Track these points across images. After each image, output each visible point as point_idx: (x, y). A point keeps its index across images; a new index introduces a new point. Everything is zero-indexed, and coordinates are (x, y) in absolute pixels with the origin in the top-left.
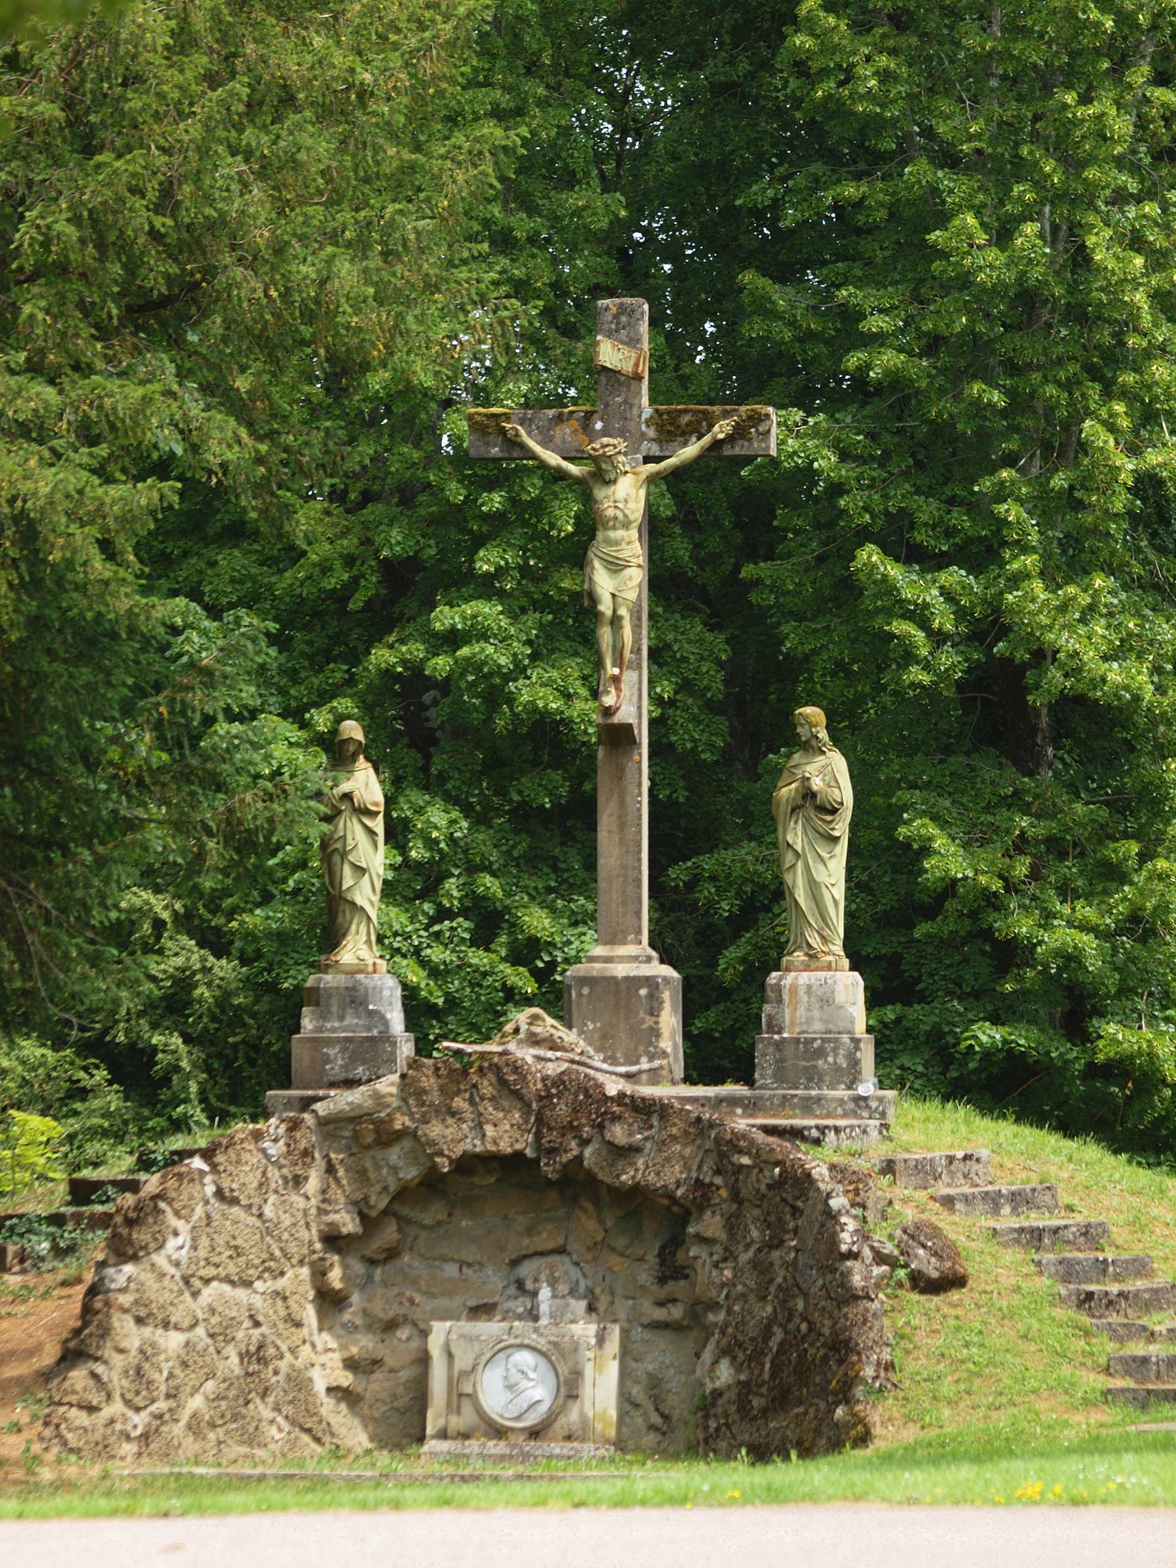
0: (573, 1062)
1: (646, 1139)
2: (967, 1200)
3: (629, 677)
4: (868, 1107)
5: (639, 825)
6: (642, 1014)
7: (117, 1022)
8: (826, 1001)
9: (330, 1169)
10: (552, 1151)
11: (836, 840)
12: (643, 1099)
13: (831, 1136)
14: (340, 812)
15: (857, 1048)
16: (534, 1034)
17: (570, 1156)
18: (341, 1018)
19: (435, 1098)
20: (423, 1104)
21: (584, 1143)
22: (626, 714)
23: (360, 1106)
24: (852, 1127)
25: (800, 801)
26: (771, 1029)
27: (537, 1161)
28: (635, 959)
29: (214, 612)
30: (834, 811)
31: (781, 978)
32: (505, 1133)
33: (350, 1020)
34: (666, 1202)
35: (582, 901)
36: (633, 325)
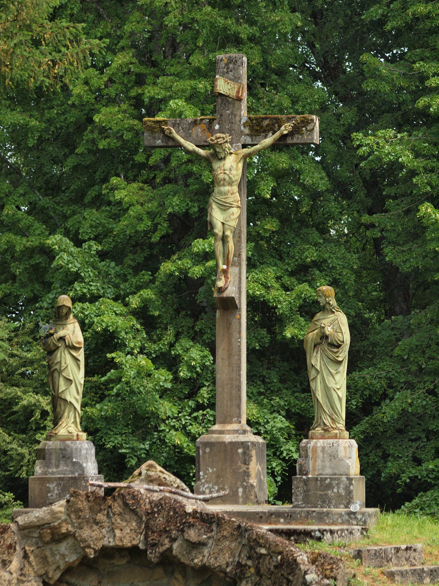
0: (171, 492)
1: (209, 538)
2: (402, 574)
3: (233, 271)
4: (356, 518)
7: (22, 466)
8: (333, 456)
9: (26, 556)
10: (154, 545)
11: (340, 363)
12: (207, 514)
13: (328, 536)
14: (58, 348)
15: (351, 484)
16: (149, 476)
17: (164, 548)
18: (57, 466)
19: (87, 514)
20: (79, 517)
21: (173, 540)
22: (231, 292)
23: (43, 519)
24: (342, 530)
25: (319, 341)
26: (301, 473)
27: (146, 551)
28: (236, 432)
29: (78, 243)
30: (339, 346)
31: (307, 443)
32: (127, 534)
33: (62, 468)
34: (222, 575)
35: (278, 399)
36: (236, 69)
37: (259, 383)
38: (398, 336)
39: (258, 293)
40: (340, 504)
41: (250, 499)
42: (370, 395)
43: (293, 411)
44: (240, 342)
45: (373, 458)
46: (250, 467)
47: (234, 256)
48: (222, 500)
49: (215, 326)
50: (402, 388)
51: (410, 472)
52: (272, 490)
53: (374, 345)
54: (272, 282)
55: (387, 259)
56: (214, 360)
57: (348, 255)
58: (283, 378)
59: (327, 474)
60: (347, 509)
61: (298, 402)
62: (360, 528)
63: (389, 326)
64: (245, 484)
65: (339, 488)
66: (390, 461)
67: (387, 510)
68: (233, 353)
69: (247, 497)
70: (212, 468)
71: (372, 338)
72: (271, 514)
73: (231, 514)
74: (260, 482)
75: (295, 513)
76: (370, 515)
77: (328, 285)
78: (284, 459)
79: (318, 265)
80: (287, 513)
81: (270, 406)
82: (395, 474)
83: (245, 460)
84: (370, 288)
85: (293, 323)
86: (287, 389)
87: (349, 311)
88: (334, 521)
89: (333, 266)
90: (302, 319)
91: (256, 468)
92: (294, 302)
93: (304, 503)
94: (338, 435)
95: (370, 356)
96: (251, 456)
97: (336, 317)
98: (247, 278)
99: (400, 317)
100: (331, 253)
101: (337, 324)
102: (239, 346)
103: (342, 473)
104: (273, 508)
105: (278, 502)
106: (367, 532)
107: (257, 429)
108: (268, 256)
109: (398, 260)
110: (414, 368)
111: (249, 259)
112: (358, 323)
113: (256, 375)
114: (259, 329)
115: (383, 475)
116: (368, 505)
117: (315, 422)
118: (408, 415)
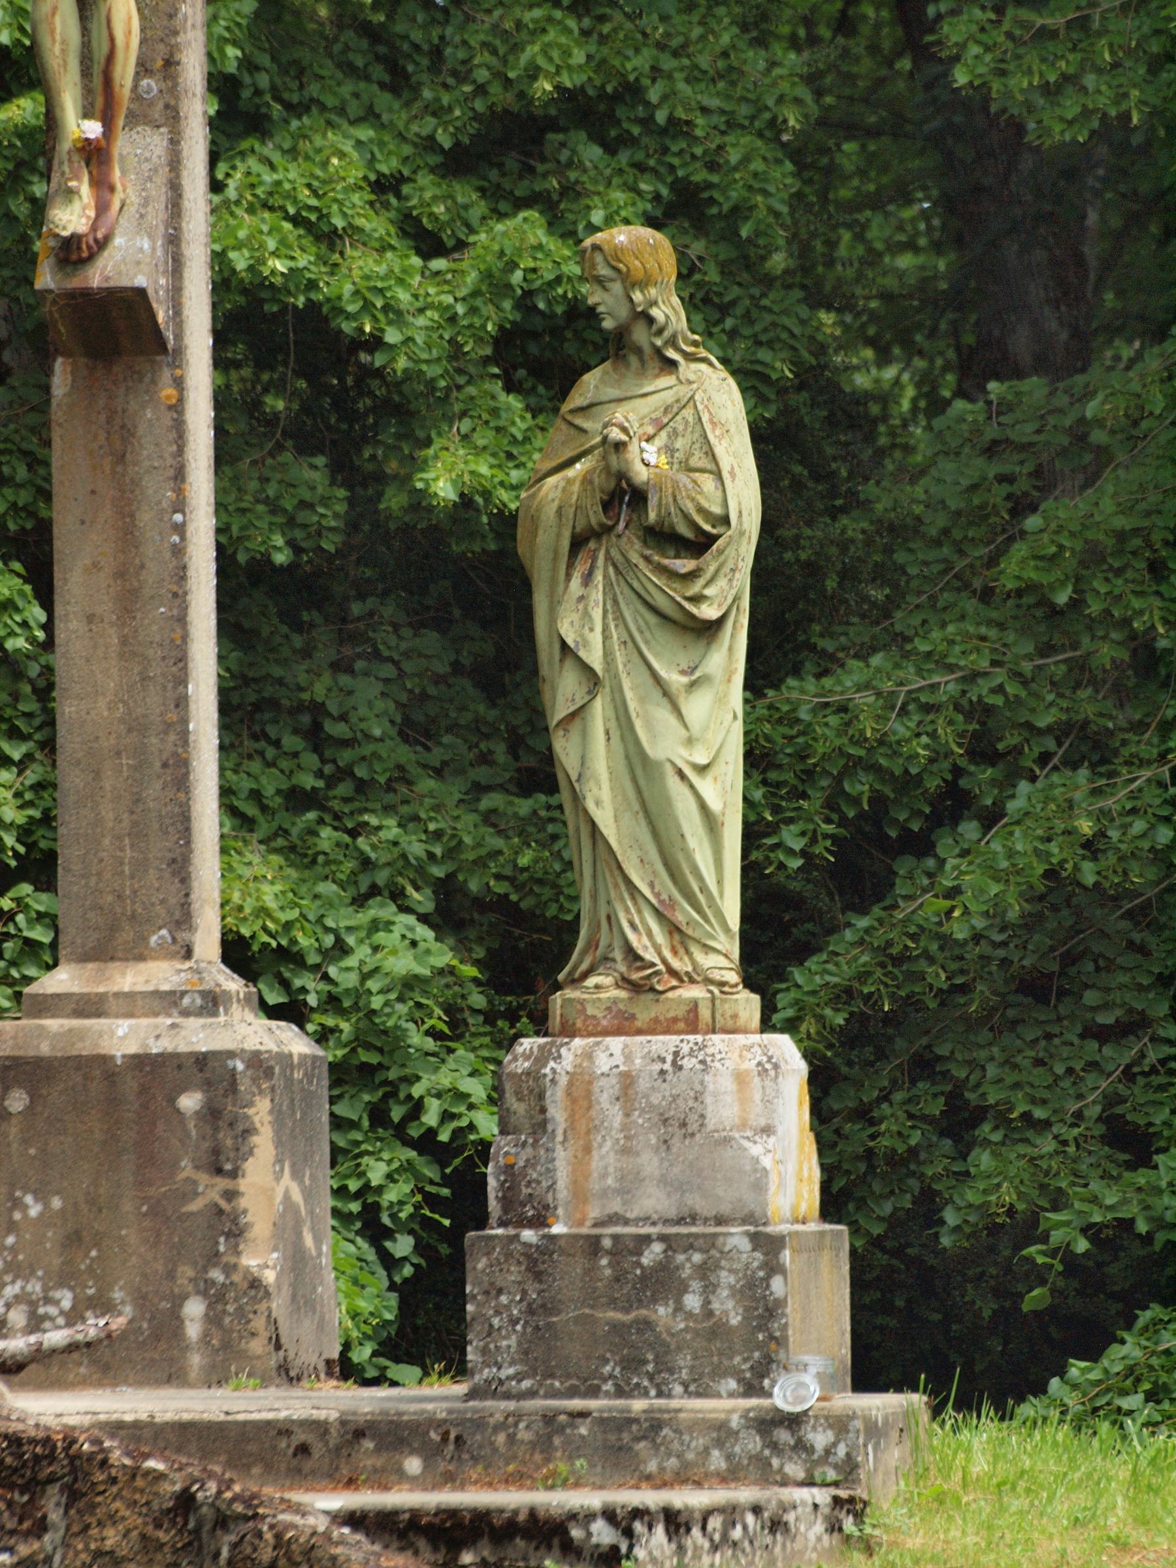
3: (139, 148)
4: (801, 1446)
5: (180, 599)
6: (186, 1169)
8: (680, 1124)
11: (709, 630)
15: (773, 1268)
22: (128, 260)
24: (731, 1513)
25: (596, 516)
26: (514, 1216)
30: (701, 544)
31: (543, 1056)
35: (391, 830)
37: (291, 742)
38: (1023, 485)
39: (280, 266)
40: (719, 1373)
41: (243, 1356)
42: (877, 799)
43: (474, 886)
44: (180, 529)
45: (894, 1129)
46: (243, 1184)
47: (143, 68)
48: (97, 1361)
49: (47, 443)
50: (1044, 759)
51: (1094, 1200)
52: (364, 1305)
53: (900, 531)
54: (355, 210)
55: (961, 77)
56: (48, 627)
57: (754, 60)
58: (418, 716)
59: (646, 1219)
60: (754, 1402)
61: (498, 843)
62: (823, 1496)
63: (977, 431)
64: (217, 1275)
65: (710, 1289)
66: (986, 1142)
67: (967, 1404)
68: (139, 588)
69: (226, 1346)
70: (41, 1195)
71: (883, 498)
72: (356, 1432)
73: (138, 1434)
74: (298, 1263)
75: (479, 1424)
76: (874, 1431)
77: (653, 222)
78: (427, 1143)
79: (598, 111)
80: (440, 1424)
81: (349, 865)
82: (1011, 1211)
83: (216, 1152)
84: (878, 231)
85: (465, 425)
86: (438, 773)
87: (764, 355)
88: (686, 1465)
89: (671, 119)
90: (515, 402)
91: (276, 1189)
92: (473, 310)
93: (531, 1373)
94: (705, 1013)
95: (878, 594)
96: (249, 1131)
97: (684, 391)
98: (216, 186)
99: (1034, 387)
100: (661, 46)
101: (692, 427)
102: (179, 551)
103: (725, 1209)
104: (366, 1401)
105: (396, 1371)
106: (859, 1517)
107: (285, 984)
108: (328, 69)
109: (1019, 82)
110: (1107, 652)
111: (221, 85)
112: (813, 418)
113: (274, 704)
114: (287, 457)
115: (951, 1217)
116: (867, 1373)
117: (580, 944)
118: (1080, 899)
